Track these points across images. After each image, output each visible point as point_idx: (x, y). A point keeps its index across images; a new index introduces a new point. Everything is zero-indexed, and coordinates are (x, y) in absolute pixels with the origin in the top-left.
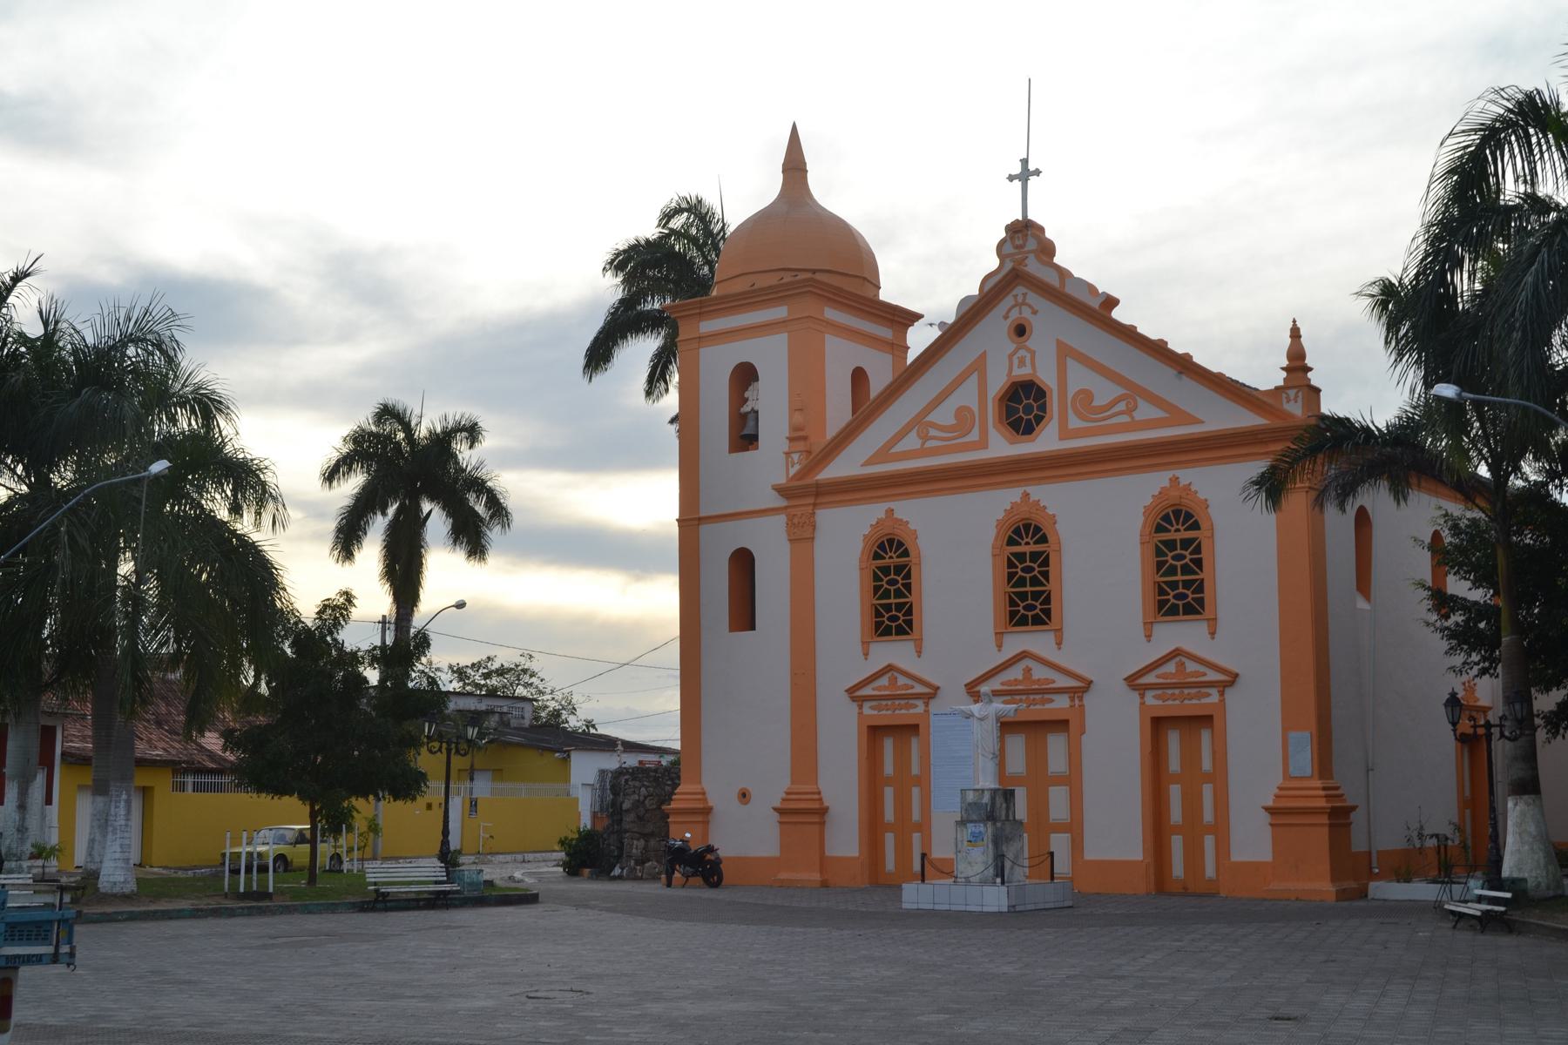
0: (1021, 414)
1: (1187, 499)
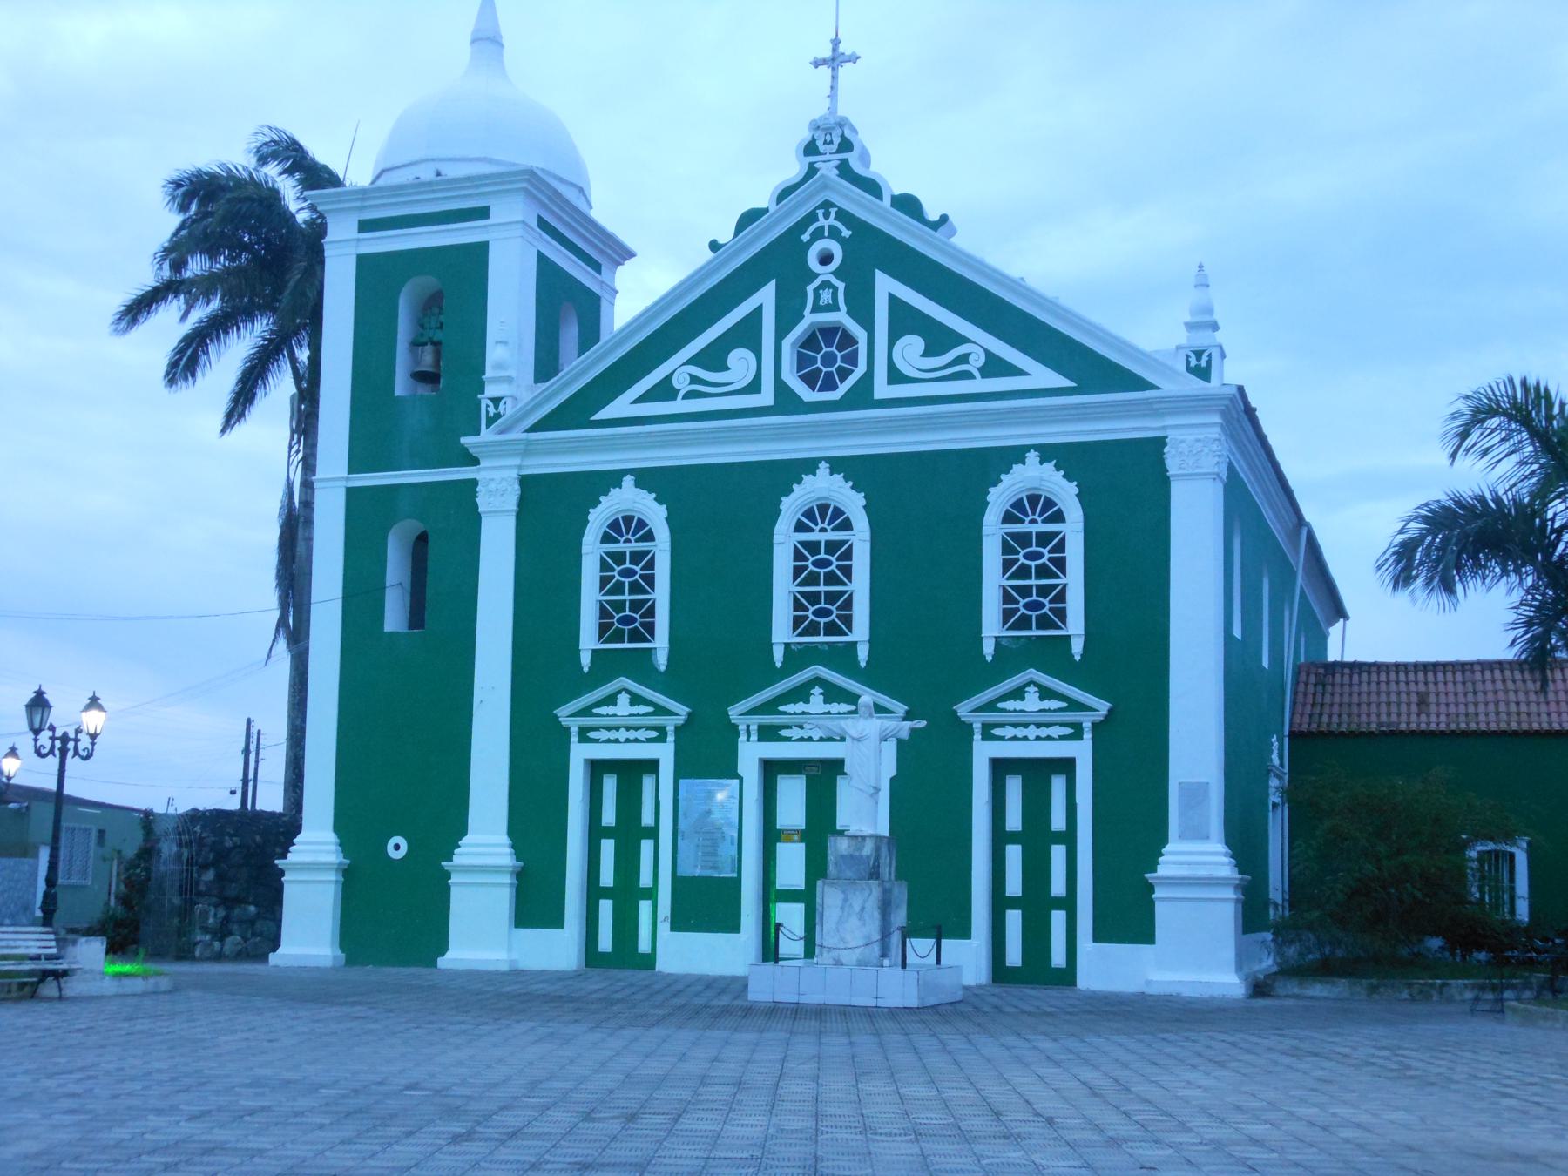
0: (819, 365)
1: (1049, 481)
